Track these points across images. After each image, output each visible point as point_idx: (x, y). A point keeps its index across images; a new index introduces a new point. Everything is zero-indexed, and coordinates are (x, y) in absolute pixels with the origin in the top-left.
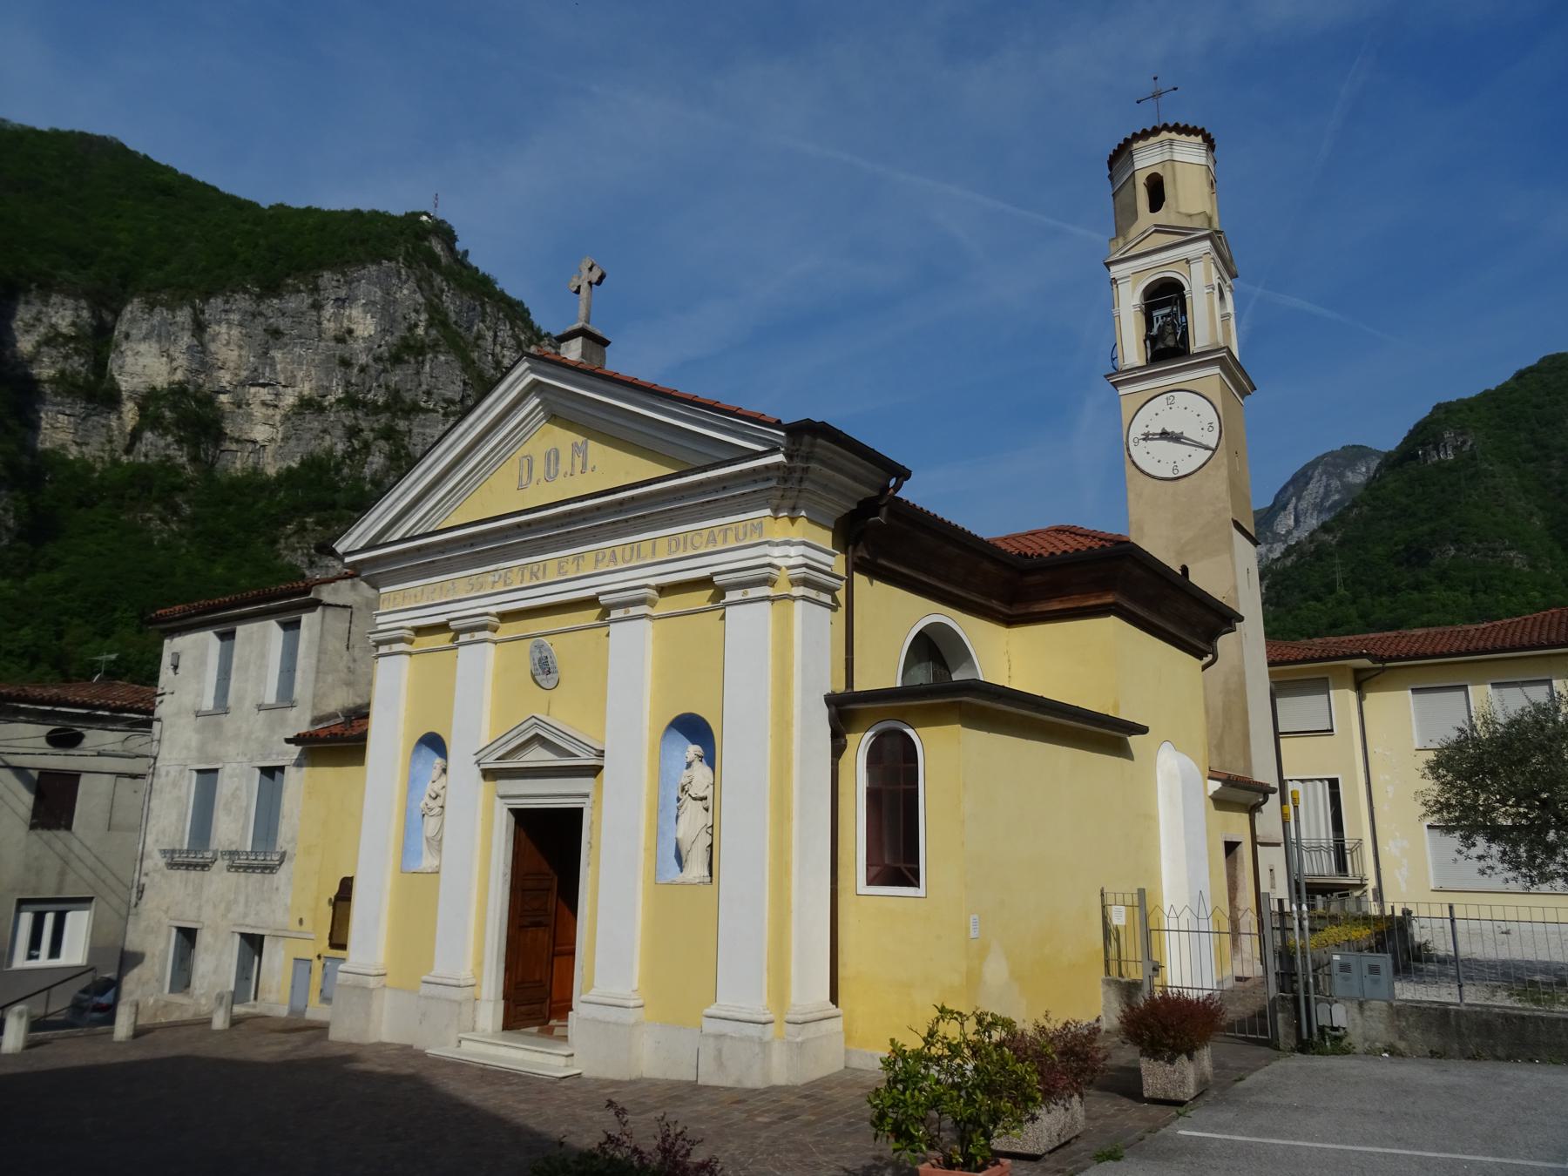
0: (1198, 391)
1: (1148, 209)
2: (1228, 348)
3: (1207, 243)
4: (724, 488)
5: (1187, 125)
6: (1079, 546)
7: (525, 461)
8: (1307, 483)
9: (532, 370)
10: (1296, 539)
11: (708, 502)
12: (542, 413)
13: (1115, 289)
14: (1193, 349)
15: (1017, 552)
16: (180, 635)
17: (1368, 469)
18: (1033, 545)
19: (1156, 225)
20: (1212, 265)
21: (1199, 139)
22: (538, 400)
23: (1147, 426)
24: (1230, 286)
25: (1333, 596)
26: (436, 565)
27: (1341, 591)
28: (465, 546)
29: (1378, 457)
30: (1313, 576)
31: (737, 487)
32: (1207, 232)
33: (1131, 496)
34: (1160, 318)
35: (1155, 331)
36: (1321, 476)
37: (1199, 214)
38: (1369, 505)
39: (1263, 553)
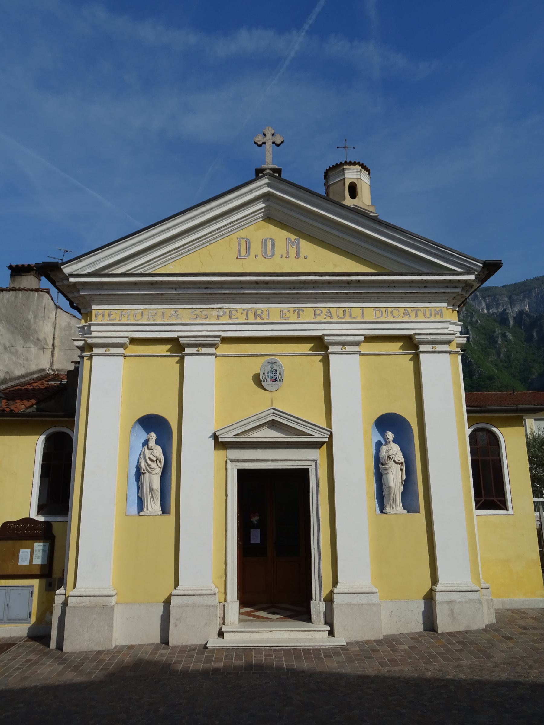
4: (425, 287)
7: (243, 243)
9: (268, 185)
11: (410, 293)
12: (262, 214)
22: (264, 205)
26: (163, 296)
28: (172, 288)
31: (433, 287)
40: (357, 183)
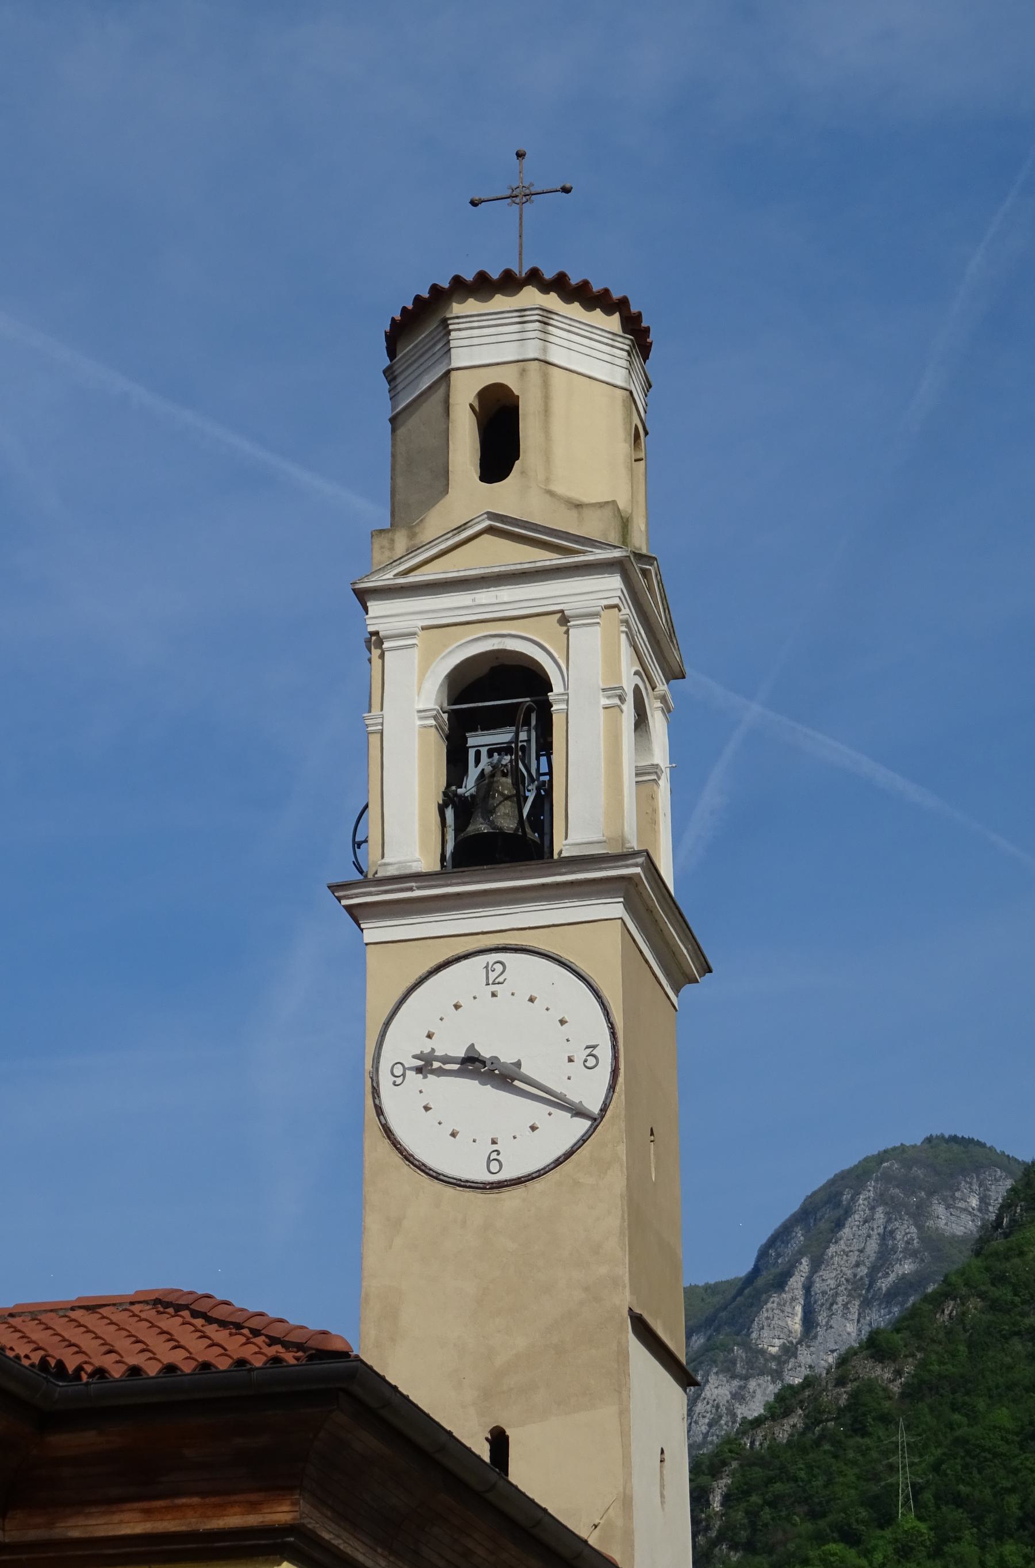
0: (566, 956)
1: (475, 473)
2: (647, 851)
3: (614, 583)
5: (606, 291)
6: (211, 1355)
8: (839, 1224)
10: (805, 1372)
13: (376, 662)
14: (563, 845)
15: (36, 1358)
16: (749, 1272)
17: (984, 1200)
18: (87, 1343)
19: (492, 516)
20: (623, 636)
21: (614, 322)
23: (430, 1036)
24: (663, 699)
25: (888, 1533)
27: (907, 1519)
29: (1010, 1173)
30: (841, 1473)
32: (617, 554)
33: (373, 1223)
34: (484, 751)
35: (469, 786)
36: (873, 1209)
37: (601, 505)
38: (982, 1296)
39: (723, 1402)
40: (516, 393)
